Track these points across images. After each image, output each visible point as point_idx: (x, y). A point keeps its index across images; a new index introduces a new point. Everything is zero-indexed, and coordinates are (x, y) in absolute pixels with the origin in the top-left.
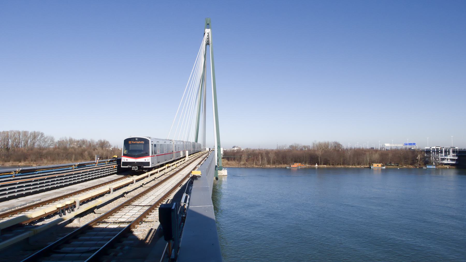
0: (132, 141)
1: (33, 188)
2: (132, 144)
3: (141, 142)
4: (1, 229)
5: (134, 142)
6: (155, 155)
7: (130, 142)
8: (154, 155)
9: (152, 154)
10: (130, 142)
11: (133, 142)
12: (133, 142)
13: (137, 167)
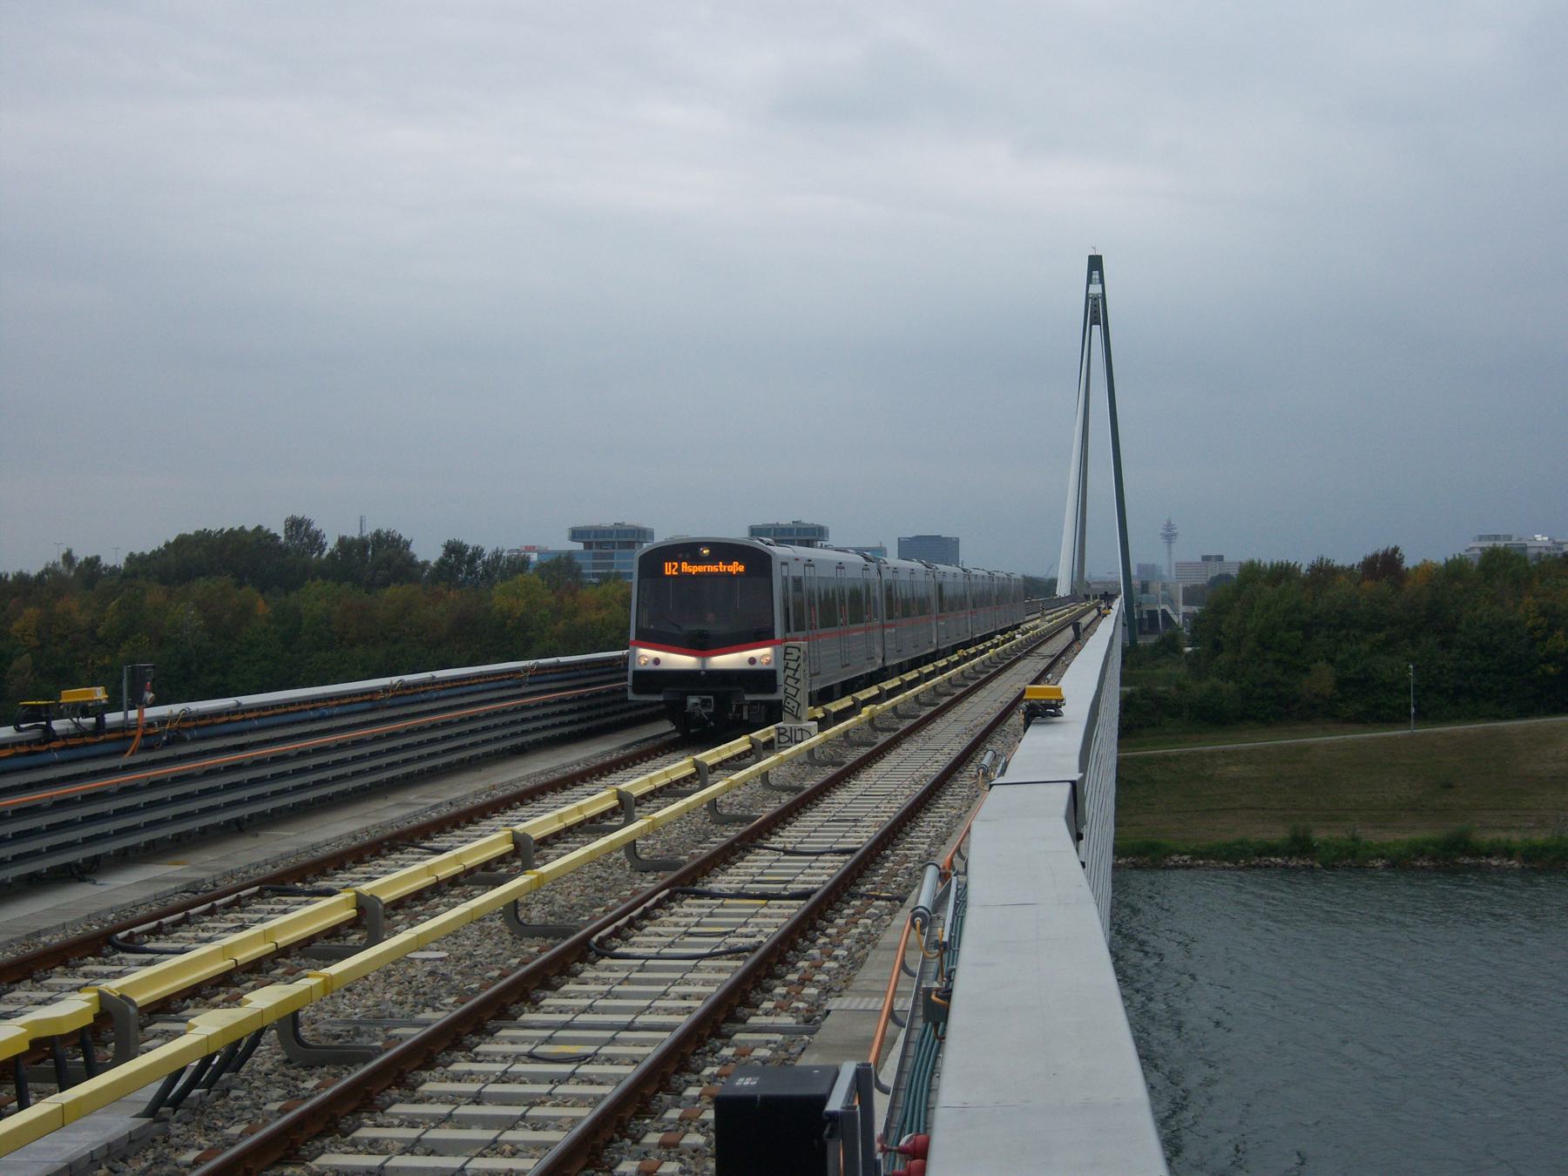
1: (53, 850)
2: (683, 576)
4: (139, 1006)
6: (800, 634)
8: (793, 634)
9: (788, 629)
10: (669, 569)
13: (711, 697)
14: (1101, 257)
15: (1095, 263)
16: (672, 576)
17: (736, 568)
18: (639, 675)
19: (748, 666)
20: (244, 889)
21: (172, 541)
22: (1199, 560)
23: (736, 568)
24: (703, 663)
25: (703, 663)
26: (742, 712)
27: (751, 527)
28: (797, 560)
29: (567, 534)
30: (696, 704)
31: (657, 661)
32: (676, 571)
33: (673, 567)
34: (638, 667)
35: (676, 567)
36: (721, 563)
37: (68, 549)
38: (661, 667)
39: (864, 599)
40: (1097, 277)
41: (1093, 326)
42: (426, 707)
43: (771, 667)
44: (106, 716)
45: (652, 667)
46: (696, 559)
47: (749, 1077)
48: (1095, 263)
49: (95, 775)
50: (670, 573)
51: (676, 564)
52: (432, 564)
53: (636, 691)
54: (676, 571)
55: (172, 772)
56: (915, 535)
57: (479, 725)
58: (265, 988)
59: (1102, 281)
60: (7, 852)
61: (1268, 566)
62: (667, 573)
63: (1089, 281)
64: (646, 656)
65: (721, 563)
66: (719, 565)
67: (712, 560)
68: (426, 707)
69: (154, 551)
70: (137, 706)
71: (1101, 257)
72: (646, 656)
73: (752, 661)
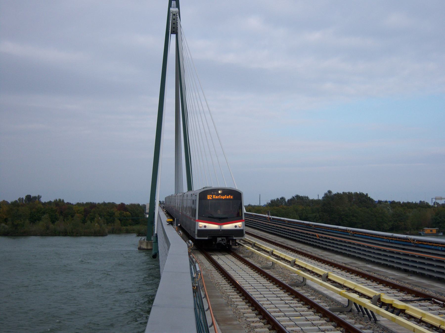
0: (212, 195)
7: (209, 197)
10: (209, 197)
11: (214, 196)
12: (214, 196)
13: (225, 238)
16: (210, 199)
18: (199, 231)
20: (248, 280)
21: (44, 200)
24: (221, 227)
25: (221, 227)
26: (230, 243)
30: (220, 240)
31: (205, 227)
33: (210, 196)
34: (199, 228)
35: (211, 196)
36: (230, 195)
37: (39, 196)
38: (207, 228)
41: (171, 34)
42: (292, 226)
43: (242, 228)
45: (203, 228)
49: (438, 255)
50: (209, 199)
52: (24, 199)
53: (198, 236)
54: (211, 198)
57: (352, 246)
58: (365, 299)
59: (178, 6)
61: (58, 200)
62: (208, 198)
63: (170, 6)
64: (201, 225)
65: (230, 195)
66: (229, 196)
68: (292, 226)
69: (83, 203)
72: (201, 225)
73: (236, 226)
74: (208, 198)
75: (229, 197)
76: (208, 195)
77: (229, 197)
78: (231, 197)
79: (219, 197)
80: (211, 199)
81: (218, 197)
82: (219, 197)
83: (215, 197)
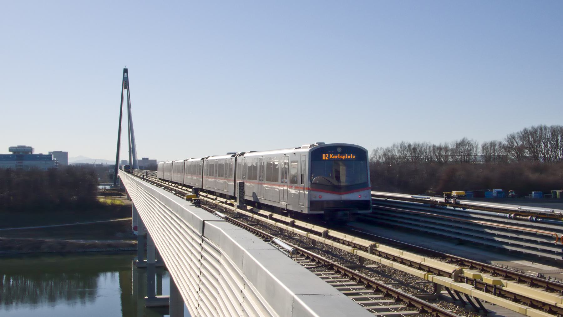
0: (329, 154)
2: (330, 160)
3: (349, 157)
5: (335, 157)
7: (325, 157)
10: (325, 157)
11: (331, 156)
12: (331, 156)
14: (127, 69)
15: (126, 71)
16: (325, 160)
17: (352, 157)
19: (300, 212)
22: (142, 159)
23: (352, 157)
27: (9, 148)
28: (294, 154)
29: (8, 150)
32: (327, 158)
33: (326, 156)
36: (351, 155)
39: (224, 168)
40: (126, 75)
44: (323, 213)
46: (336, 153)
47: (451, 293)
48: (126, 71)
50: (325, 159)
51: (327, 155)
54: (327, 158)
55: (454, 219)
56: (54, 151)
60: (560, 235)
62: (323, 159)
65: (351, 155)
67: (342, 153)
70: (561, 189)
71: (127, 69)
74: (323, 159)
75: (350, 157)
76: (323, 155)
77: (350, 157)
78: (353, 157)
79: (338, 157)
80: (328, 159)
81: (337, 156)
82: (338, 157)
83: (333, 156)
